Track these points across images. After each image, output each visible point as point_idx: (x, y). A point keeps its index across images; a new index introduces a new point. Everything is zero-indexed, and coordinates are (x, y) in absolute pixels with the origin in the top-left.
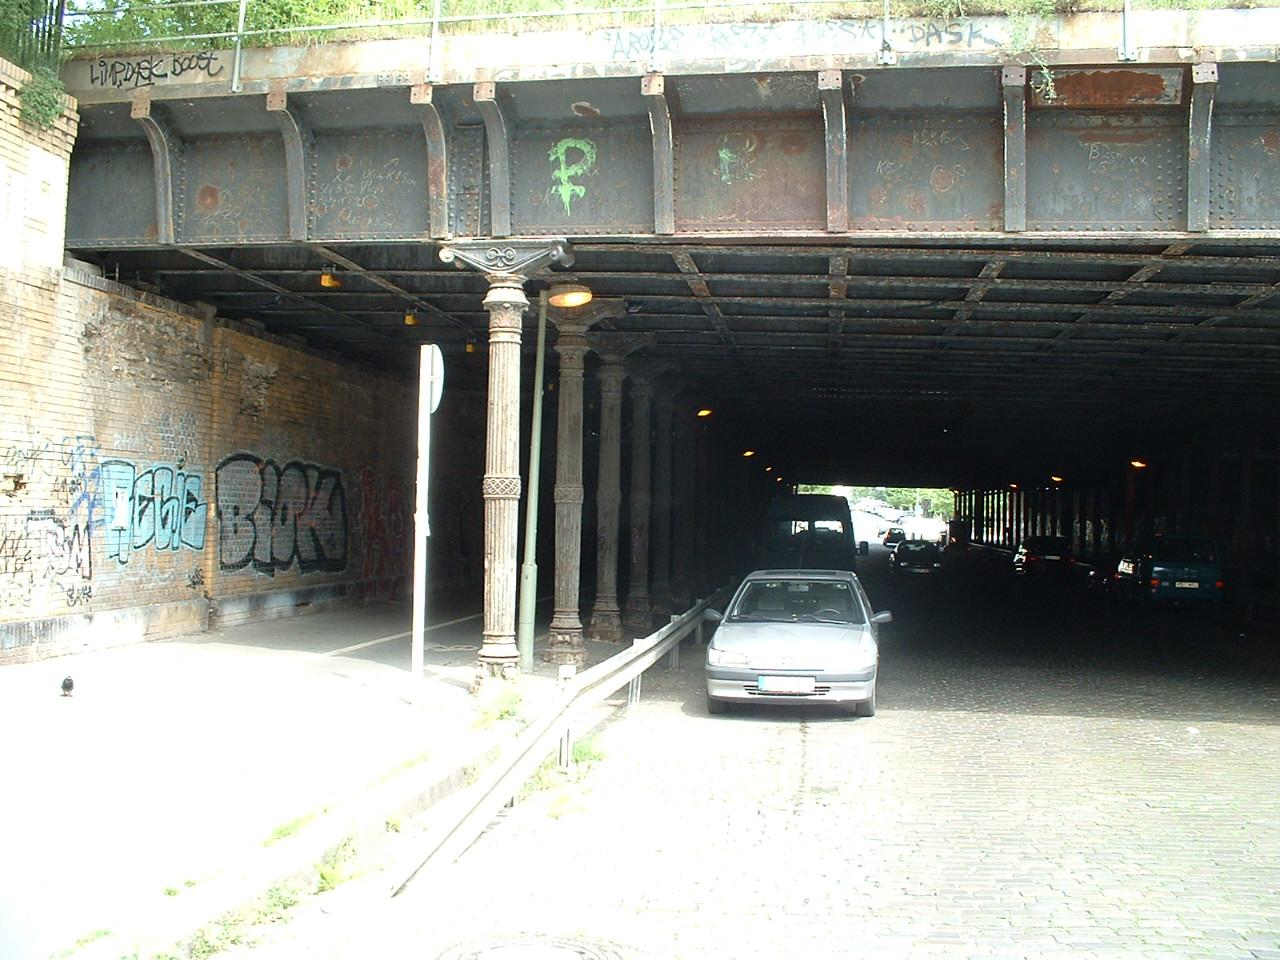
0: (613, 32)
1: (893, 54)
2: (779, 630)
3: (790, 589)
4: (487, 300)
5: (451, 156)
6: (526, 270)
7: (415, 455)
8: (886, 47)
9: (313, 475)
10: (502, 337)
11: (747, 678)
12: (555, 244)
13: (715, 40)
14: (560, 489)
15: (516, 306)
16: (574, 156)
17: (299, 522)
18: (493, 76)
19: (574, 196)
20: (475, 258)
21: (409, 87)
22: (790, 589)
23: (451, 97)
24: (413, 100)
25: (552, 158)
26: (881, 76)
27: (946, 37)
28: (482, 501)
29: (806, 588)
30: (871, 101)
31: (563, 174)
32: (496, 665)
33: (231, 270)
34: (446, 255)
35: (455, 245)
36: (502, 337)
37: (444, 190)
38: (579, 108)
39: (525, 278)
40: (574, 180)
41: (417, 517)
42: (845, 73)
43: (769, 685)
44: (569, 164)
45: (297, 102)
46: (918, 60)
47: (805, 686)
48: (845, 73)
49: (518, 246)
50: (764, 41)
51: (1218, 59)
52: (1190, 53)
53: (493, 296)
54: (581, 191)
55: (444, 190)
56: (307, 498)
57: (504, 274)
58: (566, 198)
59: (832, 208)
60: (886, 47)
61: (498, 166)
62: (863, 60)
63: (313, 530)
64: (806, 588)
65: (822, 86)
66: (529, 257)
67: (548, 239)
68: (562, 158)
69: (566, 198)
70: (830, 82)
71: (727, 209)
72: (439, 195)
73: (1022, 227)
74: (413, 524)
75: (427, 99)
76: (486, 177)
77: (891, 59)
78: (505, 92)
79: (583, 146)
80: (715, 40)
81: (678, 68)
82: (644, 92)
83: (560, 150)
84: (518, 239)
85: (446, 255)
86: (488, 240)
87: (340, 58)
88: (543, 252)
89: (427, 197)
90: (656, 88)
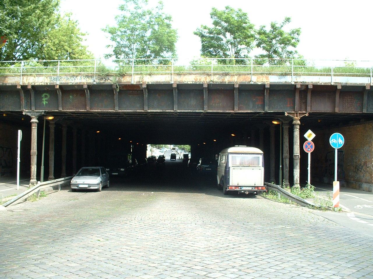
0: (51, 77)
1: (95, 82)
2: (85, 177)
3: (89, 170)
4: (31, 121)
5: (25, 96)
6: (38, 116)
7: (17, 148)
8: (94, 81)
9: (5, 149)
10: (34, 128)
11: (77, 185)
12: (42, 112)
13: (67, 79)
14: (284, 134)
15: (36, 122)
16: (46, 96)
17: (2, 159)
18: (31, 84)
19: (46, 103)
20: (29, 114)
21: (17, 85)
22: (89, 170)
23: (24, 87)
24: (17, 88)
25: (42, 97)
26: (94, 86)
27: (104, 79)
28: (30, 156)
29: (91, 170)
30: (65, 89)
31: (44, 99)
32: (33, 184)
33: (11, 113)
34: (24, 113)
35: (25, 112)
36: (34, 128)
37: (23, 102)
38: (46, 89)
39: (38, 117)
40: (46, 100)
41: (18, 158)
42: (88, 85)
43: (81, 186)
44: (45, 98)
45: (33, 87)
46: (99, 83)
47: (86, 186)
48: (88, 85)
49: (36, 112)
50: (75, 79)
51: (146, 83)
52: (142, 82)
53: (32, 120)
54: (47, 102)
55: (23, 102)
56: (3, 153)
57: (34, 117)
58: (45, 104)
59: (88, 106)
60: (94, 81)
61: (33, 98)
62: (91, 83)
63: (5, 160)
64: (91, 170)
65: (204, 86)
66: (38, 114)
67: (41, 111)
68: (44, 97)
69: (45, 104)
70: (205, 86)
71: (70, 107)
72: (23, 103)
73: (118, 110)
74: (17, 159)
75: (20, 88)
76: (31, 100)
77: (95, 83)
78: (61, 87)
79: (47, 94)
80: (67, 79)
81: (61, 84)
82: (56, 88)
83: (44, 95)
84: (36, 111)
85: (24, 113)
86: (31, 111)
87: (5, 80)
88: (40, 113)
89: (20, 103)
90: (58, 87)
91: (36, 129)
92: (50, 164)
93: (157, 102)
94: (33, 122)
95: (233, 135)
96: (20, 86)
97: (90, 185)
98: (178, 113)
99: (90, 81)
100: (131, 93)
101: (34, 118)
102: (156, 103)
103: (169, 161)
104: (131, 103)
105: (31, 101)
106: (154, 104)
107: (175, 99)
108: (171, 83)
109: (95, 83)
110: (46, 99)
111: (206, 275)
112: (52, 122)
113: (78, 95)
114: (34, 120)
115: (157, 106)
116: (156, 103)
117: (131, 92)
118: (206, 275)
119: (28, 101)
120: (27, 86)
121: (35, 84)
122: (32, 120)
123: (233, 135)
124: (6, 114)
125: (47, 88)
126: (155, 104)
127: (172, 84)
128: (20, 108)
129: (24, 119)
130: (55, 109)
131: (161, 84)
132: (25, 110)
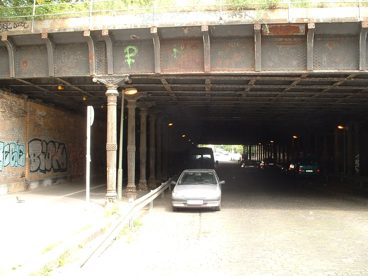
1: (223, 21)
3: (196, 175)
4: (107, 93)
6: (118, 84)
9: (57, 144)
10: (111, 103)
15: (115, 94)
16: (131, 51)
17: (53, 158)
19: (131, 62)
20: (103, 81)
21: (83, 31)
22: (196, 175)
23: (95, 34)
25: (125, 51)
27: (238, 16)
31: (128, 56)
32: (111, 198)
35: (97, 77)
36: (111, 103)
37: (94, 61)
38: (132, 37)
40: (131, 58)
43: (190, 202)
44: (130, 53)
49: (115, 77)
53: (108, 92)
54: (133, 61)
55: (94, 61)
56: (56, 151)
57: (111, 85)
58: (129, 63)
60: (221, 19)
61: (109, 54)
62: (214, 23)
63: (57, 160)
64: (200, 175)
66: (119, 80)
68: (128, 51)
69: (129, 63)
71: (176, 65)
72: (92, 62)
74: (86, 158)
75: (89, 35)
76: (106, 57)
77: (222, 22)
79: (134, 48)
81: (161, 25)
85: (94, 80)
86: (107, 75)
90: (155, 31)
91: (116, 106)
92: (128, 166)
93: (327, 56)
94: (110, 94)
95: (295, 137)
96: (89, 32)
97: (206, 201)
98: (352, 79)
99: (215, 19)
100: (281, 41)
101: (111, 87)
102: (325, 59)
103: (237, 164)
104: (281, 59)
105: (106, 60)
106: (322, 59)
107: (361, 50)
108: (359, 21)
109: (223, 23)
110: (132, 55)
111: (13, 152)
112: (132, 101)
113: (188, 47)
114: (112, 91)
115: (328, 62)
116: (325, 59)
117: (281, 39)
118: (13, 152)
119: (102, 60)
120: (101, 31)
121: (114, 27)
122: (107, 91)
123: (295, 137)
124: (62, 87)
125: (135, 36)
126: (323, 60)
127: (361, 22)
128: (88, 70)
129: (86, 98)
130: (148, 71)
131: (341, 23)
132: (96, 74)
